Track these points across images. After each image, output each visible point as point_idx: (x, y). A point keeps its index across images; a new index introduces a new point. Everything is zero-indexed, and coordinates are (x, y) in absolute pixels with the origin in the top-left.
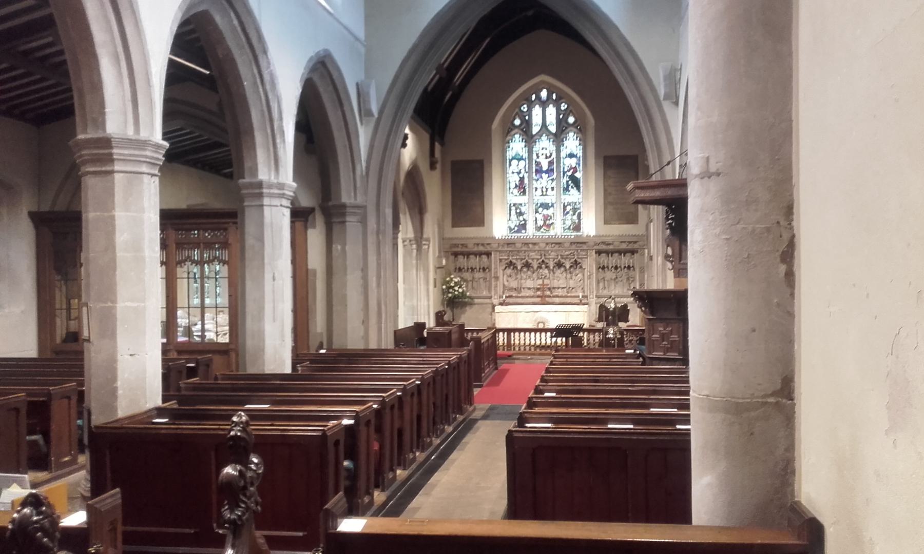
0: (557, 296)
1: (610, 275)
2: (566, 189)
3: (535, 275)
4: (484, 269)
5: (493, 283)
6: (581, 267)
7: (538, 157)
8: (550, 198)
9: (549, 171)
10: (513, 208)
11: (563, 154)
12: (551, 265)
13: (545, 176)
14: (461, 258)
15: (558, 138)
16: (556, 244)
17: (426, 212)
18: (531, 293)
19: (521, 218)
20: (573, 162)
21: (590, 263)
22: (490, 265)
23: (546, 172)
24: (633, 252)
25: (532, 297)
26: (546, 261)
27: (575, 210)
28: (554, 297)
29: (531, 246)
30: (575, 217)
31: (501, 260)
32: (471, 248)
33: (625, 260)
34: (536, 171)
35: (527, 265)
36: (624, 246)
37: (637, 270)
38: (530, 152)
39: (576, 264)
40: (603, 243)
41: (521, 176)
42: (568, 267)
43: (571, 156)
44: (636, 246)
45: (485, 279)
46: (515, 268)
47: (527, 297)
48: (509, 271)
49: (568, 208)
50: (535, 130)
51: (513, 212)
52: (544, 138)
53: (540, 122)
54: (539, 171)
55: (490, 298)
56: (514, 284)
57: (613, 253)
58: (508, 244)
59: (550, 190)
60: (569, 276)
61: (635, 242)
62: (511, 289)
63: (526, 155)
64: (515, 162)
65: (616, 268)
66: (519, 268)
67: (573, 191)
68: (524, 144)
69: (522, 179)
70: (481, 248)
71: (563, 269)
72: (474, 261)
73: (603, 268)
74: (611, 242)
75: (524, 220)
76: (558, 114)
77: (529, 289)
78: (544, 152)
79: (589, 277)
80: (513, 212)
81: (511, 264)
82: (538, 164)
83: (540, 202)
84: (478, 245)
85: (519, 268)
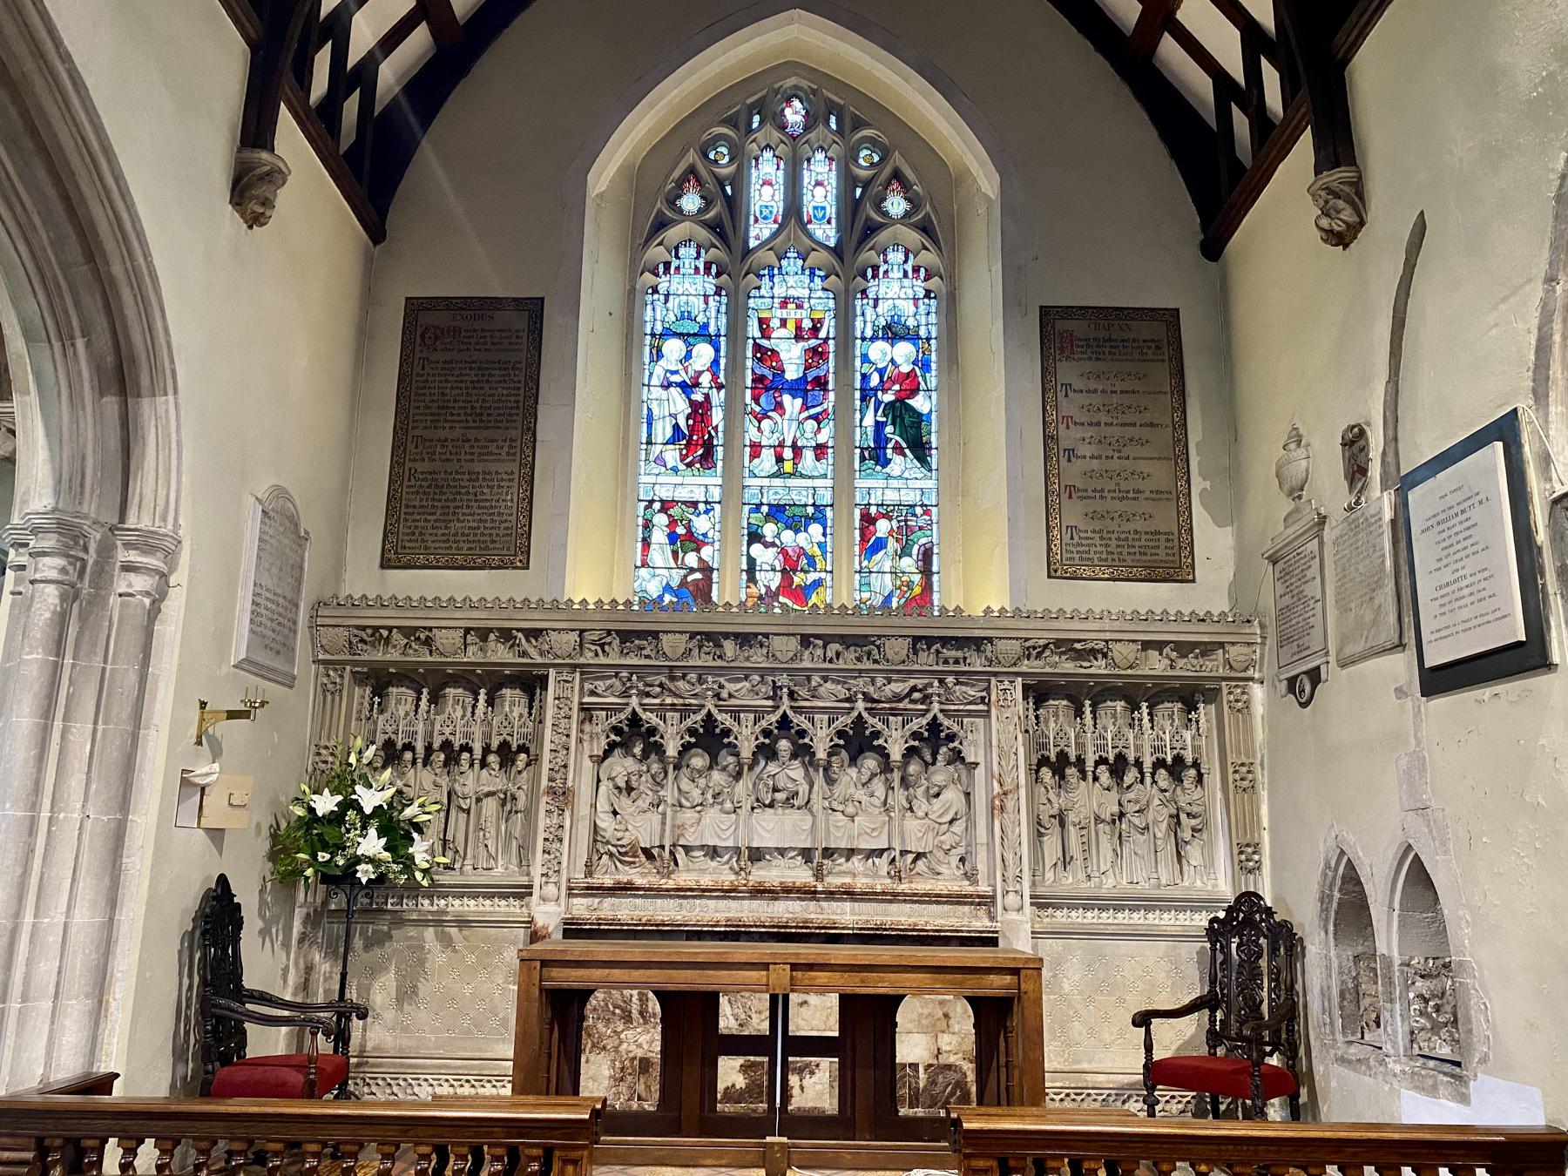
0: (850, 894)
1: (1090, 798)
2: (876, 454)
3: (742, 788)
4: (507, 754)
5: (543, 821)
6: (957, 757)
7: (766, 334)
8: (813, 483)
9: (811, 387)
10: (661, 520)
11: (867, 319)
12: (821, 740)
13: (792, 404)
14: (401, 699)
15: (851, 258)
16: (847, 641)
17: (162, 382)
18: (721, 874)
19: (691, 559)
20: (903, 353)
21: (999, 737)
22: (538, 738)
23: (798, 388)
24: (1190, 696)
25: (728, 893)
26: (799, 720)
27: (905, 534)
28: (831, 895)
29: (729, 647)
30: (908, 564)
31: (586, 710)
32: (450, 647)
33: (1160, 732)
34: (758, 379)
35: (710, 739)
36: (1156, 665)
37: (1213, 779)
38: (737, 315)
39: (934, 741)
40: (1064, 646)
41: (698, 396)
42: (896, 752)
43: (893, 332)
44: (1213, 666)
45: (507, 799)
46: (654, 749)
47: (703, 893)
48: (622, 766)
49: (882, 527)
50: (759, 232)
51: (659, 536)
52: (792, 264)
53: (778, 207)
54: (770, 384)
55: (522, 892)
56: (643, 828)
57: (1102, 692)
58: (625, 636)
59: (809, 455)
60: (899, 797)
61: (1206, 649)
62: (628, 854)
63: (718, 324)
64: (673, 348)
65: (1118, 767)
66: (672, 750)
67: (899, 464)
68: (709, 284)
69: (700, 411)
70: (500, 653)
71: (870, 763)
72: (460, 717)
73: (1059, 765)
74: (1096, 639)
75: (706, 569)
76: (848, 180)
77: (713, 852)
78: (791, 313)
79: (997, 808)
80: (659, 536)
81: (633, 735)
82: (765, 355)
83: (770, 498)
84: (483, 634)
85: (672, 750)
